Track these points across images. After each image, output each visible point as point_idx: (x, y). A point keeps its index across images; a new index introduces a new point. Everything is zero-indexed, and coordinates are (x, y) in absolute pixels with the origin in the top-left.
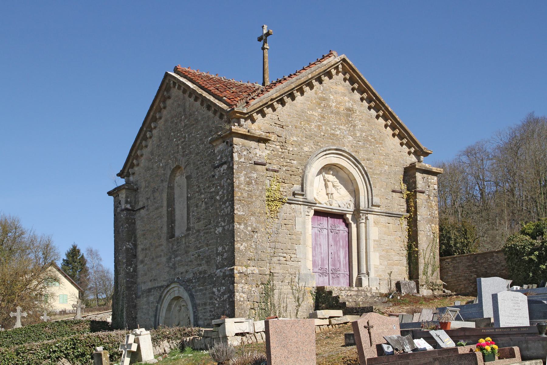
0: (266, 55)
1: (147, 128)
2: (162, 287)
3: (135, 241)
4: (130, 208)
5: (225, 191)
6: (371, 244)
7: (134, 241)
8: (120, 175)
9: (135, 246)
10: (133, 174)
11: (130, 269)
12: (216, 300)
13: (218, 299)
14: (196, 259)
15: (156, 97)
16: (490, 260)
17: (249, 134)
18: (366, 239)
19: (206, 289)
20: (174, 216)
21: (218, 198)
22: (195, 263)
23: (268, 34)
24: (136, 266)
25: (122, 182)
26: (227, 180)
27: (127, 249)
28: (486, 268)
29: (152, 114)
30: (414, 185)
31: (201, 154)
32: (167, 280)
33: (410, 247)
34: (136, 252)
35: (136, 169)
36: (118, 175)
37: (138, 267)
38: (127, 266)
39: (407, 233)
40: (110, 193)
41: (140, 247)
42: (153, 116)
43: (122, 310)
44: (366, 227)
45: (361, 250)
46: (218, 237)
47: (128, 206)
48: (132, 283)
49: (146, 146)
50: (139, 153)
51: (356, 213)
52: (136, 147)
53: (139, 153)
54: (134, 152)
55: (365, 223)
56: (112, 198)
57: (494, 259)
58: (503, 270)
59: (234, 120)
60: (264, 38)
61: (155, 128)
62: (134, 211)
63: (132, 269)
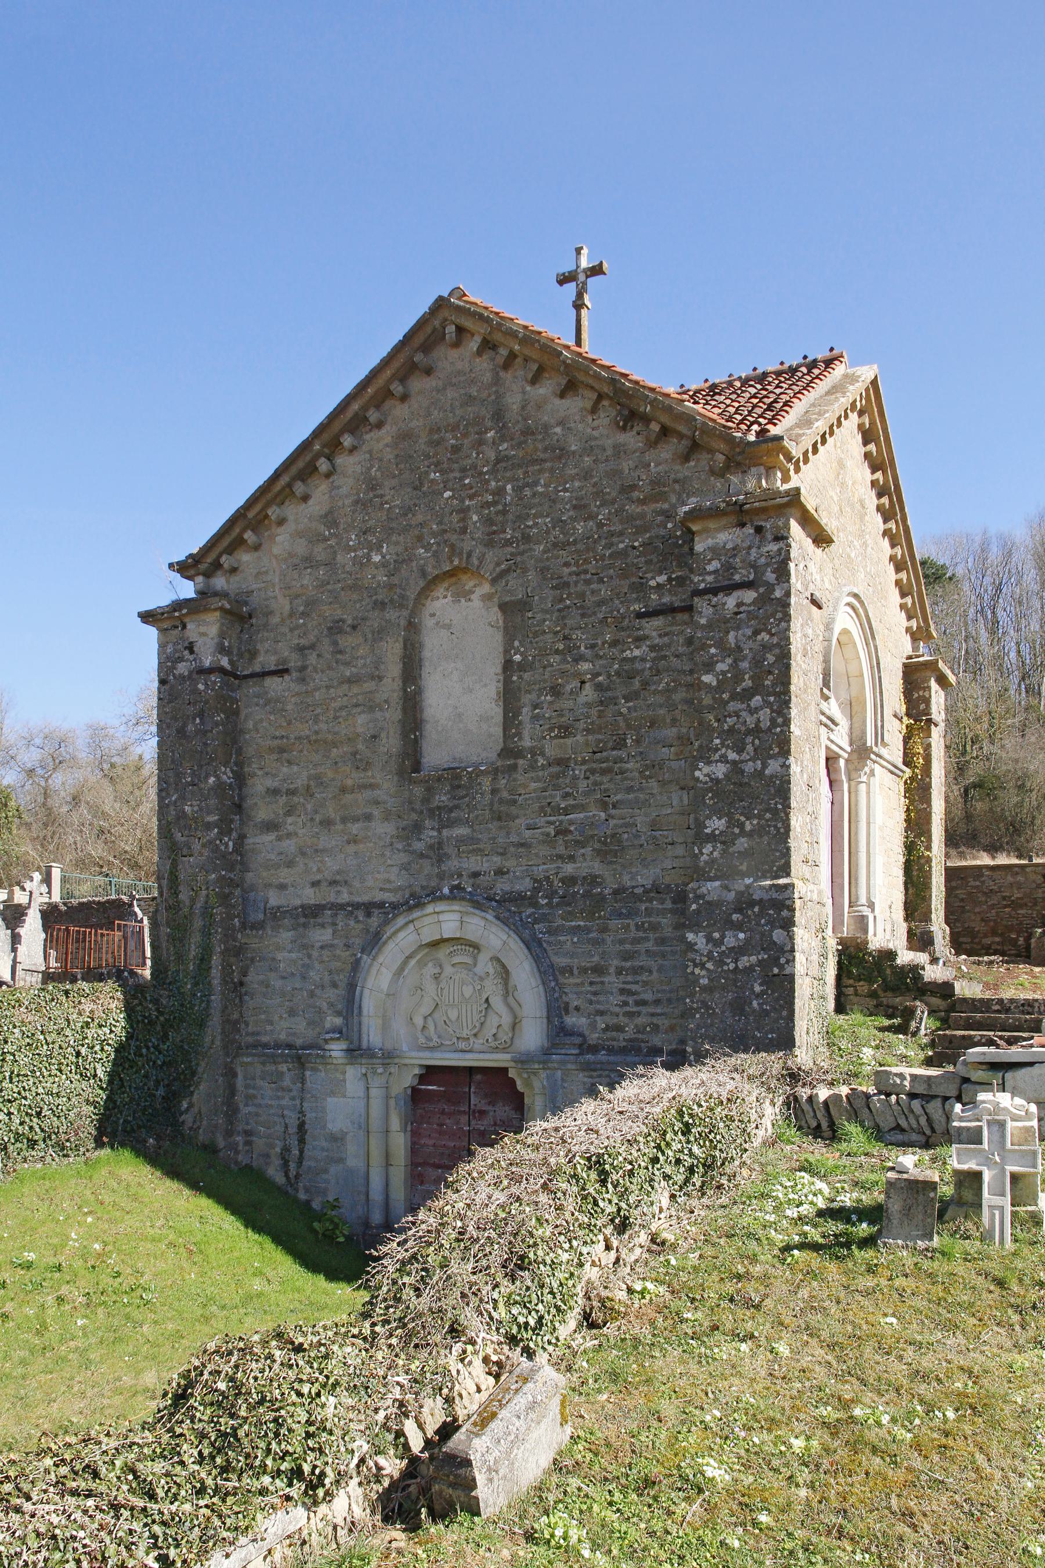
0: (585, 322)
1: (324, 446)
2: (381, 905)
3: (240, 764)
4: (228, 667)
5: (745, 665)
6: (876, 833)
7: (236, 764)
8: (185, 568)
9: (241, 779)
10: (234, 570)
11: (227, 844)
12: (702, 966)
13: (710, 965)
14: (549, 841)
15: (385, 363)
16: (972, 883)
17: (813, 512)
18: (868, 823)
19: (604, 930)
20: (422, 711)
21: (707, 678)
22: (544, 851)
23: (596, 270)
24: (242, 837)
25: (187, 590)
26: (756, 633)
27: (220, 785)
28: (962, 900)
29: (355, 407)
30: (922, 706)
31: (580, 546)
32: (400, 888)
33: (910, 848)
34: (242, 798)
35: (245, 557)
36: (171, 566)
37: (249, 841)
38: (221, 833)
39: (903, 816)
40: (147, 617)
41: (259, 785)
42: (356, 414)
43: (204, 960)
44: (868, 793)
45: (857, 846)
46: (710, 790)
47: (225, 662)
48: (233, 884)
49: (305, 498)
50: (273, 512)
51: (855, 756)
52: (269, 496)
53: (273, 512)
54: (258, 507)
55: (868, 785)
56: (151, 633)
57: (983, 882)
58: (1006, 906)
59: (762, 469)
60: (582, 277)
61: (353, 450)
62: (236, 677)
63: (231, 844)
